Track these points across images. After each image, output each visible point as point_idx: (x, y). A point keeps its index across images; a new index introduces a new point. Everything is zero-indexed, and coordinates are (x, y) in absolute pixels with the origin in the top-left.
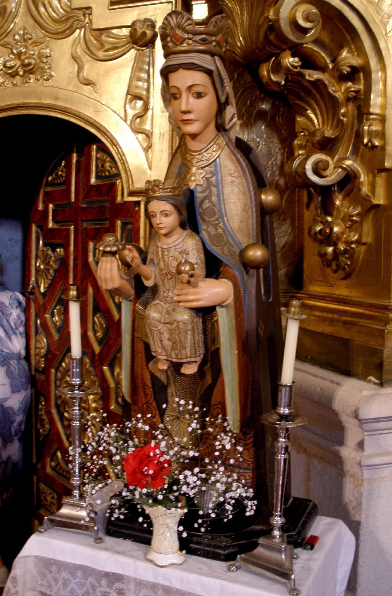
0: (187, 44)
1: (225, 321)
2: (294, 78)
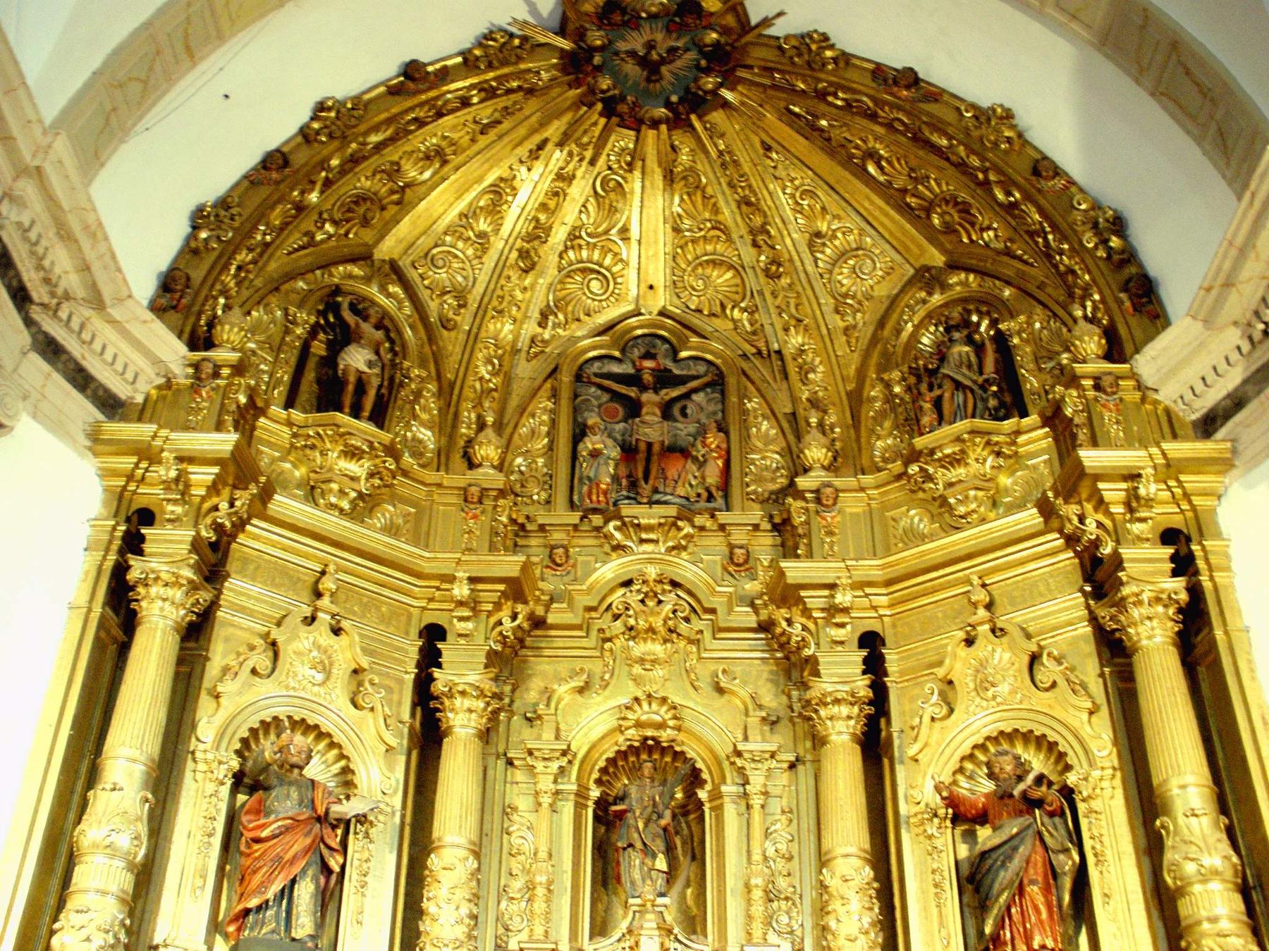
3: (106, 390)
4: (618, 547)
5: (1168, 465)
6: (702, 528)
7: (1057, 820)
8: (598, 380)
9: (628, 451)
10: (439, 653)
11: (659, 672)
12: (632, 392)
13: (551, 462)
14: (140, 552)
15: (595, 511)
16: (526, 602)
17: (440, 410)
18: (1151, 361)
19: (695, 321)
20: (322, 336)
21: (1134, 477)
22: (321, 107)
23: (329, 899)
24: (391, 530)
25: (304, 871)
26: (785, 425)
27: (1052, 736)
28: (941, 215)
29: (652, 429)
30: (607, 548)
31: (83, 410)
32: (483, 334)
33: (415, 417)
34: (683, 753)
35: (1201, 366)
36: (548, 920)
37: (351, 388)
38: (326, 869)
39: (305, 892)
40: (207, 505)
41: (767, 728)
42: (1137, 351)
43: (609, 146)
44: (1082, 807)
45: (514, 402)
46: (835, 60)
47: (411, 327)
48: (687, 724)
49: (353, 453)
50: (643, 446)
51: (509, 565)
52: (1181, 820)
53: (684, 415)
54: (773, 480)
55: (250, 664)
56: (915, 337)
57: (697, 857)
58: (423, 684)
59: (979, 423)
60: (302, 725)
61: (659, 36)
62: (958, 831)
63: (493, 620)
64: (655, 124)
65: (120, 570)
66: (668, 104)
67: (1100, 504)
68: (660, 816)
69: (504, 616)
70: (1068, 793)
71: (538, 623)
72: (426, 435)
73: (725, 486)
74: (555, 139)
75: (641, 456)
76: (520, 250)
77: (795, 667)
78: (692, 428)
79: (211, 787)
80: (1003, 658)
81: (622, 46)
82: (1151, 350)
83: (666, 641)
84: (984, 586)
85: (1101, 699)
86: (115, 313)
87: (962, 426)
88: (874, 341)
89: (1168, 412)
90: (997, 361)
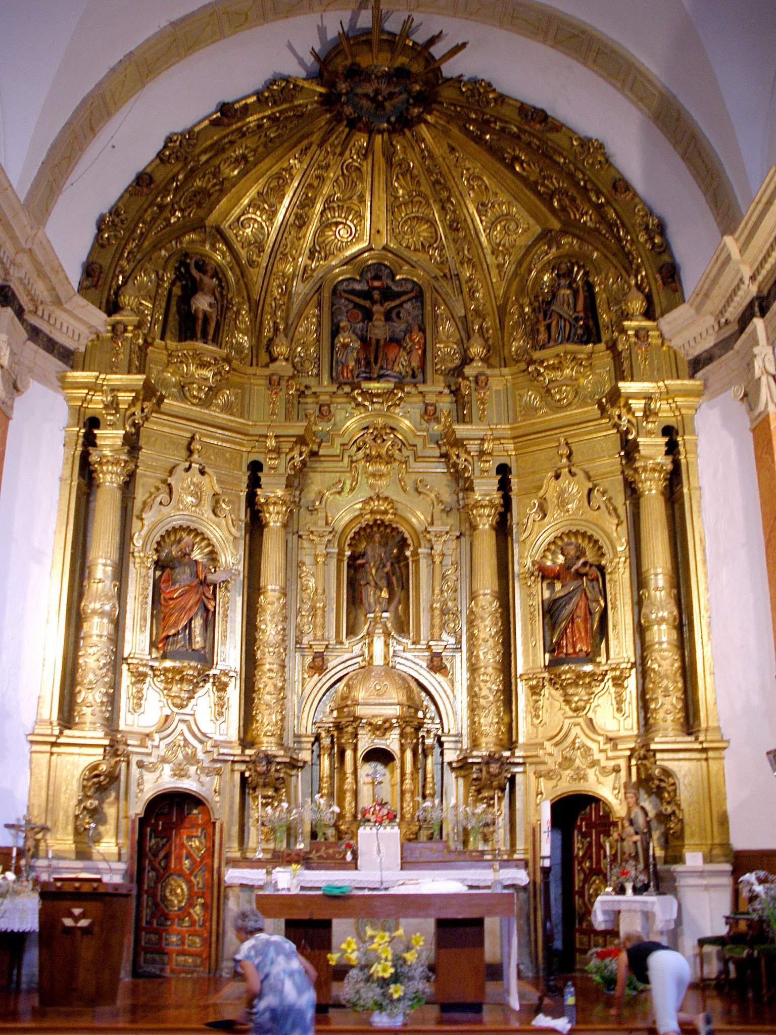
0: (451, 336)
1: (639, 844)
2: (658, 787)
3: (64, 347)
4: (358, 405)
5: (667, 392)
6: (409, 393)
7: (595, 583)
8: (347, 295)
9: (364, 341)
10: (259, 479)
11: (383, 482)
12: (367, 304)
13: (319, 350)
14: (95, 445)
15: (345, 384)
16: (307, 445)
17: (251, 321)
18: (670, 322)
19: (406, 253)
20: (178, 284)
21: (649, 398)
22: (169, 139)
23: (209, 624)
24: (227, 408)
25: (196, 614)
27: (596, 537)
28: (558, 201)
29: (379, 330)
30: (353, 405)
31: (53, 363)
32: (275, 270)
33: (237, 328)
34: (397, 528)
35: (693, 332)
36: (323, 627)
37: (200, 322)
38: (207, 610)
39: (198, 623)
40: (129, 413)
41: (444, 515)
42: (662, 315)
43: (352, 143)
44: (608, 577)
45: (295, 308)
46: (495, 100)
47: (231, 269)
48: (399, 512)
49: (203, 365)
50: (374, 342)
51: (297, 428)
52: (653, 592)
54: (452, 361)
55: (158, 499)
56: (539, 278)
57: (405, 587)
58: (251, 498)
59: (570, 347)
60: (189, 530)
61: (383, 86)
63: (289, 457)
64: (381, 132)
66: (389, 122)
67: (629, 410)
68: (384, 566)
69: (296, 453)
70: (602, 569)
71: (314, 454)
72: (244, 340)
73: (423, 367)
74: (318, 142)
75: (373, 348)
76: (296, 215)
77: (461, 481)
78: (403, 327)
79: (144, 571)
80: (575, 488)
81: (359, 91)
82: (669, 317)
83: (387, 463)
84: (567, 444)
85: (623, 517)
86: (67, 306)
87: (560, 349)
88: (515, 274)
89: (675, 353)
90: (585, 298)
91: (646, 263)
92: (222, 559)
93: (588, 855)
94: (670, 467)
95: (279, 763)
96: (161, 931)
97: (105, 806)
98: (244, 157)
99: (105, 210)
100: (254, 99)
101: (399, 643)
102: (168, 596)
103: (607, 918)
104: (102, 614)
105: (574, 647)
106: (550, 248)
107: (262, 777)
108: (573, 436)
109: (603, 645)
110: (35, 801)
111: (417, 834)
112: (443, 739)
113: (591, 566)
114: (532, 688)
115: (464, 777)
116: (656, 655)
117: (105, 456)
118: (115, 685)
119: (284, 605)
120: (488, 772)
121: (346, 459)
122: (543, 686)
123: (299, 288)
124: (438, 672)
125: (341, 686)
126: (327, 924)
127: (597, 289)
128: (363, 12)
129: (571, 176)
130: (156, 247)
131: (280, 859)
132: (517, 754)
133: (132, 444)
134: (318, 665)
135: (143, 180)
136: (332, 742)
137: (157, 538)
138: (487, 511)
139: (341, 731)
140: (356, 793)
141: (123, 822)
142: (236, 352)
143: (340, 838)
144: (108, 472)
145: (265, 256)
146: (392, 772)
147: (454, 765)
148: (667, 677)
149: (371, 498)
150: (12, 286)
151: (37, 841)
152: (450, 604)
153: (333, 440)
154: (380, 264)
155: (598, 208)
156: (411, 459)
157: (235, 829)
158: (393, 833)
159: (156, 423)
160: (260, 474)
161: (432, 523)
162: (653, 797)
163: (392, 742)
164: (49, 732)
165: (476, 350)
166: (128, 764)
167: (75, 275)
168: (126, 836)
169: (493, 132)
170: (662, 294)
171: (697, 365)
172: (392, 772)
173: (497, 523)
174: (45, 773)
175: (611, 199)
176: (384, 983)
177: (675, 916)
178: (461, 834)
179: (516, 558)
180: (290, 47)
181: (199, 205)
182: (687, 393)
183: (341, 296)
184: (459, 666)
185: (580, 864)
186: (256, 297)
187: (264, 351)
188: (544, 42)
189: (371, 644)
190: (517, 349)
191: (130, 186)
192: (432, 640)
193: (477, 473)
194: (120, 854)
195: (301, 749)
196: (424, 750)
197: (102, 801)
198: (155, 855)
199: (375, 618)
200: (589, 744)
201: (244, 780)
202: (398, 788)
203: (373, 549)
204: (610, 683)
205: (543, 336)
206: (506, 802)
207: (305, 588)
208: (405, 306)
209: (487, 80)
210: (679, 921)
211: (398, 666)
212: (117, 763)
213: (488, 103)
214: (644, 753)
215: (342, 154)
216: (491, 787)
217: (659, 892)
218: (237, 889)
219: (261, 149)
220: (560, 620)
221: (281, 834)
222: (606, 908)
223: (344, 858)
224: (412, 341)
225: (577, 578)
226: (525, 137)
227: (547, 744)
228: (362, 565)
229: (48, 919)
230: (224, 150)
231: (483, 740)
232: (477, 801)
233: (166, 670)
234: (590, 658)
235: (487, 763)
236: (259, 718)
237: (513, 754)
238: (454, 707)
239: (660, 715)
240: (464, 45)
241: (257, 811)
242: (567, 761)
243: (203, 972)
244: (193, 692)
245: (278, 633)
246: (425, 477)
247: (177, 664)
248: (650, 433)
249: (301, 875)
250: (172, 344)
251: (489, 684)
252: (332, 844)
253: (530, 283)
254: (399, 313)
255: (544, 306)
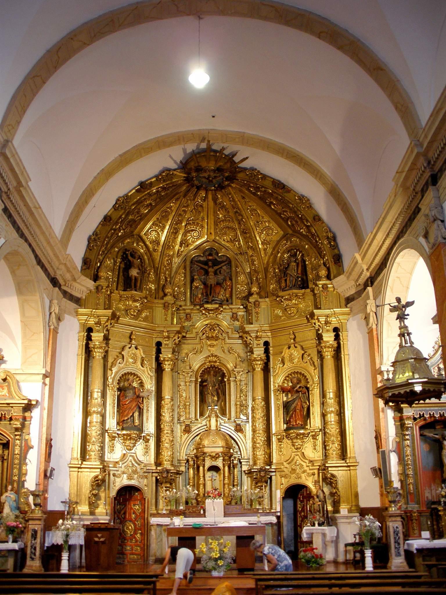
9: (205, 284)
10: (160, 350)
12: (206, 267)
14: (91, 340)
15: (197, 305)
16: (181, 334)
20: (123, 263)
21: (327, 316)
22: (118, 200)
24: (146, 319)
25: (136, 411)
26: (247, 276)
28: (291, 222)
29: (212, 280)
30: (201, 314)
32: (165, 253)
37: (133, 281)
38: (140, 408)
39: (136, 414)
40: (105, 325)
44: (310, 392)
45: (174, 269)
46: (262, 178)
49: (135, 301)
53: (220, 273)
55: (118, 362)
57: (224, 394)
58: (157, 358)
60: (131, 374)
62: (284, 395)
63: (173, 339)
65: (87, 345)
66: (214, 187)
68: (215, 386)
69: (176, 337)
70: (308, 389)
75: (209, 288)
78: (222, 277)
80: (296, 353)
83: (216, 340)
87: (290, 292)
88: (272, 254)
90: (302, 266)
91: (327, 254)
92: (146, 386)
93: (303, 510)
94: (336, 345)
95: (172, 473)
96: (122, 545)
97: (100, 493)
98: (151, 204)
99: (91, 234)
100: (154, 179)
101: (222, 419)
102: (124, 403)
103: (308, 536)
104: (97, 413)
105: (296, 423)
106: (287, 242)
107: (165, 479)
108: (296, 330)
109: (308, 421)
110: (72, 491)
111: (230, 502)
112: (241, 461)
113: (303, 388)
114: (278, 439)
115: (250, 477)
116: (329, 427)
117: (96, 345)
118: (103, 442)
119: (173, 405)
120: (260, 476)
121: (198, 338)
122: (283, 438)
123: (176, 261)
124: (240, 429)
125: (198, 438)
126: (194, 539)
127: (307, 263)
128: (202, 143)
129: (295, 212)
130: (113, 247)
131: (172, 514)
132: (272, 467)
133: (106, 338)
134: (187, 430)
135: (107, 219)
136: (194, 463)
137: (118, 378)
138: (259, 363)
139: (198, 459)
140: (204, 485)
141: (108, 499)
142: (149, 292)
143: (198, 504)
144: (97, 352)
145: (160, 248)
146: (220, 475)
147: (246, 472)
148: (333, 436)
149: (209, 356)
150: (57, 277)
151: (74, 508)
152: (244, 402)
153: (192, 331)
154: (212, 248)
155: (308, 227)
156: (227, 338)
157: (154, 501)
158: (220, 502)
159: (116, 328)
160: (161, 347)
161: (235, 367)
162: (329, 485)
163: (219, 463)
164: (77, 463)
165: (255, 289)
166: (109, 474)
167: (79, 264)
168: (109, 505)
169: (261, 191)
170: (334, 267)
171: (349, 300)
172: (220, 475)
173: (264, 367)
174: (76, 480)
175: (312, 224)
176: (216, 560)
177: (336, 535)
178: (249, 501)
179: (272, 383)
180: (170, 156)
181: (131, 226)
182: (343, 314)
183: (194, 264)
184: (248, 429)
185: (300, 514)
186: (157, 266)
187: (161, 292)
188: (282, 157)
189: (210, 421)
190: (273, 288)
191: (101, 221)
192: (236, 418)
193: (255, 346)
194: (107, 513)
195: (181, 466)
196: (233, 466)
197: (99, 491)
198: (120, 513)
199: (211, 409)
200: (302, 463)
201: (157, 480)
202: (222, 482)
203: (211, 378)
204: (311, 438)
205: (283, 284)
206: (268, 488)
207: (181, 396)
208: (223, 268)
209: (258, 169)
210: (338, 537)
211: (222, 430)
212: (105, 475)
213: (258, 179)
214: (323, 468)
215: (194, 200)
216: (261, 482)
217: (329, 525)
218: (155, 527)
219: (158, 200)
220: (290, 410)
221: (173, 503)
222: (308, 532)
223: (200, 512)
224: (226, 284)
225: (298, 391)
226: (275, 195)
227: (285, 463)
228: (206, 385)
229: (88, 539)
230: (142, 202)
231: (258, 461)
232: (255, 487)
233: (124, 435)
234: (303, 427)
235: (260, 472)
236: (163, 453)
237: (271, 468)
238: (246, 445)
239: (331, 452)
240: (247, 158)
241: (163, 493)
242: (293, 471)
243: (141, 562)
244: (135, 443)
245: (170, 417)
246: (232, 345)
247: (128, 432)
248: (328, 331)
249: (184, 520)
250: (122, 293)
251: (260, 438)
252: (195, 507)
253: (278, 258)
254: (220, 272)
255: (284, 271)
